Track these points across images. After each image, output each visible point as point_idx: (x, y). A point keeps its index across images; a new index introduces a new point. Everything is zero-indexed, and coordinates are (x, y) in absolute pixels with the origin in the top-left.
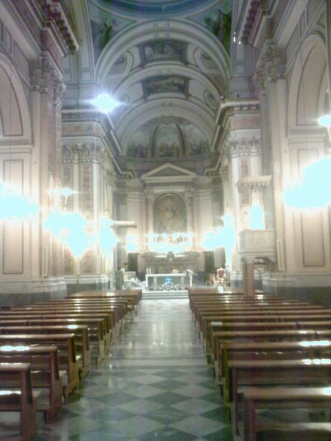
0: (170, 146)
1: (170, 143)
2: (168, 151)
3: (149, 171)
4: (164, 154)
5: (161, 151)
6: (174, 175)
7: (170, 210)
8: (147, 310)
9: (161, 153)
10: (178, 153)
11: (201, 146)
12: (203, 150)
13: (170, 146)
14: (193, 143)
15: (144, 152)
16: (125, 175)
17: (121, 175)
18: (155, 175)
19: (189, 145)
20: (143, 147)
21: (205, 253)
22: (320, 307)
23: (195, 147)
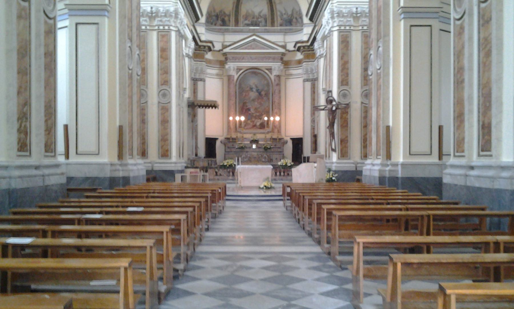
0: (256, 14)
1: (257, 11)
2: (255, 19)
3: (383, 72)
4: (249, 23)
5: (246, 20)
6: (234, 48)
7: (254, 90)
8: (239, 171)
9: (247, 22)
10: (266, 22)
11: (292, 15)
12: (294, 20)
13: (256, 14)
14: (284, 12)
15: (226, 19)
16: (205, 47)
17: (200, 46)
18: (277, 49)
19: (279, 13)
20: (225, 13)
21: (321, 218)
22: (406, 191)
23: (285, 16)
